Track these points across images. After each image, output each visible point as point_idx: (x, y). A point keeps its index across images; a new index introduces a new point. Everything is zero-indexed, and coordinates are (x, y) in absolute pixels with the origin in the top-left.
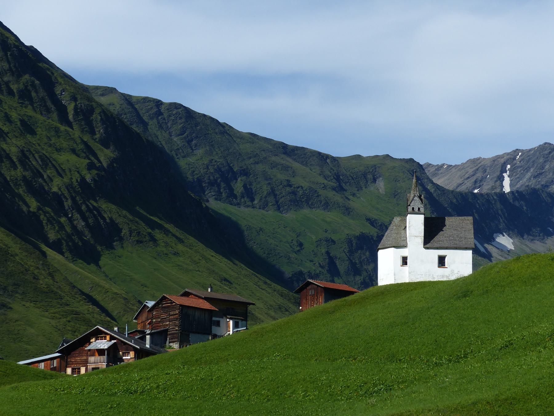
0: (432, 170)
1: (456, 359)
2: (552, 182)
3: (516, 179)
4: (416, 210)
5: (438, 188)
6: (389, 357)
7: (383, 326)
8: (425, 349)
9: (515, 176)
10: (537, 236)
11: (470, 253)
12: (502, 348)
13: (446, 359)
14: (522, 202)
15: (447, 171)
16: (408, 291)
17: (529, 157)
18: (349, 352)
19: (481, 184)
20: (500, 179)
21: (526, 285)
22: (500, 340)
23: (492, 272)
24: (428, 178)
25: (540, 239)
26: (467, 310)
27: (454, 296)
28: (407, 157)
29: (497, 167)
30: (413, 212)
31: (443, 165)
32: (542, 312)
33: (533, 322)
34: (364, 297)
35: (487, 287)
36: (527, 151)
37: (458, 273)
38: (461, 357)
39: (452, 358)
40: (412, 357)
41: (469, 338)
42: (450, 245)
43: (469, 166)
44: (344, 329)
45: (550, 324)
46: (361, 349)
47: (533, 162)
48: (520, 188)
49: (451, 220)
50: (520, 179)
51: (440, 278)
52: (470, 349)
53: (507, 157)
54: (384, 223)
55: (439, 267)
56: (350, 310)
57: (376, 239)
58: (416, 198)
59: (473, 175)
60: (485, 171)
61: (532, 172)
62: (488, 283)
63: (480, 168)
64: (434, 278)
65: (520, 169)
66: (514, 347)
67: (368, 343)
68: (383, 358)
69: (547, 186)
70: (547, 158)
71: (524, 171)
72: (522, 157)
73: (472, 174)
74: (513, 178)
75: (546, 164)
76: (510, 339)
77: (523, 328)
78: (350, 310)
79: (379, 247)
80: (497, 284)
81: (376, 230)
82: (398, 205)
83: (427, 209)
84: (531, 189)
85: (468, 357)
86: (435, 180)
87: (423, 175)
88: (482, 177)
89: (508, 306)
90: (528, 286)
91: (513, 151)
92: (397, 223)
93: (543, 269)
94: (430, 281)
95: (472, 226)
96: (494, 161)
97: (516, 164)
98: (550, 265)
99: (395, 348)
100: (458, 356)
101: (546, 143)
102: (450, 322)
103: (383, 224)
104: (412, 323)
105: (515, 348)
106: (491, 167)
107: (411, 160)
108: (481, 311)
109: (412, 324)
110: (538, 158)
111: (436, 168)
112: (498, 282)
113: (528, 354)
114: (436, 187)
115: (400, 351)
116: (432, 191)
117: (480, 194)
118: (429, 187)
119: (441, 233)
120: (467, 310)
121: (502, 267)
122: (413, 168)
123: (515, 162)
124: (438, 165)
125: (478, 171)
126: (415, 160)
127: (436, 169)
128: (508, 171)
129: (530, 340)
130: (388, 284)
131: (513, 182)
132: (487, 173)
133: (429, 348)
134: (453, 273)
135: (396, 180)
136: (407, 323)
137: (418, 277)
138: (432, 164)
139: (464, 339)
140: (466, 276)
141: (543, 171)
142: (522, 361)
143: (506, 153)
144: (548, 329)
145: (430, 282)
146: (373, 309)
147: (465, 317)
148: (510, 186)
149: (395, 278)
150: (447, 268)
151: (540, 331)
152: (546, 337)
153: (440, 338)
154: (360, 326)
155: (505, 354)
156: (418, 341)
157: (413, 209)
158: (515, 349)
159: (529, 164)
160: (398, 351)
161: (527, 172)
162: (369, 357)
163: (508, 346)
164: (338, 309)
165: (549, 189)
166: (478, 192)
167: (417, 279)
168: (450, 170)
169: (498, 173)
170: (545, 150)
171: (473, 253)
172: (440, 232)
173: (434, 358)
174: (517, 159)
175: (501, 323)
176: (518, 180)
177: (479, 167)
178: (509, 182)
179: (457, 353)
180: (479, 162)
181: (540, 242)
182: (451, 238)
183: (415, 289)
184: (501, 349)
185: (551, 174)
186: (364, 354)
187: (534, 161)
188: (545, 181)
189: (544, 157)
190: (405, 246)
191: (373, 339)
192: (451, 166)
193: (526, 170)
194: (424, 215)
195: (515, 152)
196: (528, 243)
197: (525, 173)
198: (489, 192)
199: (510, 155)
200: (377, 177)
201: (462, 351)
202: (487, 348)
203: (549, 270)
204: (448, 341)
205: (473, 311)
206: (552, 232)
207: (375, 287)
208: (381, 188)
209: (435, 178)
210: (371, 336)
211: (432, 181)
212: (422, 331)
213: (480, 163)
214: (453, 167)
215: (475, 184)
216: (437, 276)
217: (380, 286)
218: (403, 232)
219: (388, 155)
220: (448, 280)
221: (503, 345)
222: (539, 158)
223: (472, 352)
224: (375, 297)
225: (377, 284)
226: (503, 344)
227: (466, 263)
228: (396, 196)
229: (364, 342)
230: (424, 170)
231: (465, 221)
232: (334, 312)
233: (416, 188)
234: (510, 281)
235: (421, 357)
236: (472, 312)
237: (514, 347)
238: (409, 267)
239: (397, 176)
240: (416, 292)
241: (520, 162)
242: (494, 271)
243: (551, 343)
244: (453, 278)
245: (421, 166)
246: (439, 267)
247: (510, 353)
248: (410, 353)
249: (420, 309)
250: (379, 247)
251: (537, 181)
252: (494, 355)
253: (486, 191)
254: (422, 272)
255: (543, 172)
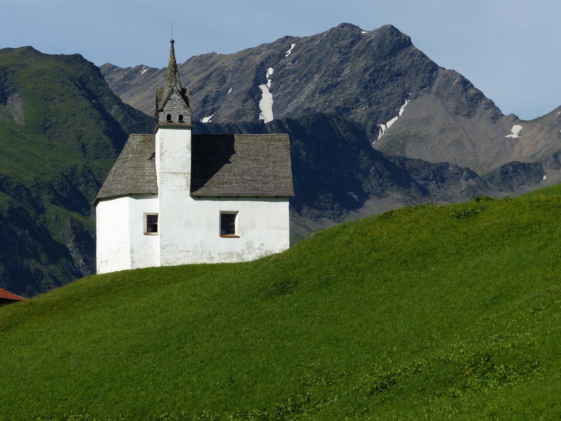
0: (118, 78)
1: (276, 415)
2: (357, 103)
3: (285, 96)
4: (175, 119)
5: (131, 114)
6: (135, 414)
7: (117, 354)
8: (210, 397)
9: (284, 90)
10: (327, 209)
11: (285, 205)
12: (374, 391)
13: (255, 415)
14: (298, 142)
15: (148, 80)
16: (160, 284)
17: (310, 53)
18: (49, 407)
19: (216, 106)
20: (253, 96)
21: (408, 268)
22: (368, 376)
23: (335, 243)
24: (111, 94)
25: (334, 214)
26: (291, 319)
27: (260, 291)
28: (69, 51)
29: (249, 71)
30: (169, 124)
31: (140, 67)
32: (447, 319)
33: (431, 339)
34: (70, 298)
35: (327, 273)
36: (307, 39)
37: (262, 247)
38: (287, 411)
39: (268, 415)
40: (183, 413)
41: (301, 373)
42: (245, 190)
43: (190, 71)
44: (36, 361)
45: (469, 343)
46: (75, 399)
47: (319, 62)
48: (293, 114)
49: (245, 141)
50: (293, 95)
51: (224, 259)
52: (304, 394)
53: (268, 52)
54: (23, 183)
55: (222, 235)
56: (43, 324)
57: (8, 216)
58: (174, 96)
59: (201, 88)
60: (223, 80)
61: (316, 83)
62: (330, 264)
63: (214, 74)
64: (212, 258)
65: (292, 76)
66: (399, 388)
67: (90, 388)
68: (123, 416)
69: (346, 110)
70: (346, 54)
71: (301, 79)
72: (297, 52)
73: (197, 85)
74: (278, 94)
75: (344, 66)
76: (389, 373)
77: (413, 352)
78: (43, 324)
79: (99, 195)
80: (348, 266)
81: (8, 198)
82: (51, 148)
83: (110, 156)
84: (316, 115)
85: (303, 412)
86: (125, 99)
87: (101, 88)
88: (218, 91)
89: (373, 310)
90: (412, 270)
91: (280, 39)
92: (135, 147)
93: (440, 237)
94: (205, 264)
95: (289, 153)
96: (241, 60)
97: (285, 66)
98: (454, 226)
99: (146, 397)
100: (281, 408)
101: (344, 25)
102: (257, 343)
103: (22, 185)
104: (177, 346)
105: (401, 389)
106: (235, 71)
107: (78, 58)
108: (319, 320)
109: (178, 349)
110: (328, 54)
111: (126, 73)
112: (351, 263)
113: (430, 401)
114: (128, 112)
115: (157, 402)
116: (120, 119)
117: (215, 125)
118: (113, 111)
119: (226, 166)
120: (291, 319)
121: (355, 232)
122: (82, 74)
123: (283, 61)
124: (130, 68)
125: (210, 81)
126: (86, 57)
127: (127, 76)
128: (269, 81)
129: (431, 374)
130: (119, 270)
131: (278, 102)
132: (226, 85)
133: (219, 395)
134: (250, 247)
135: (47, 98)
136: (167, 346)
137: (179, 256)
138: (117, 67)
139: (290, 375)
140: (279, 254)
141: (339, 79)
142: (423, 414)
143: (264, 44)
144: (467, 352)
145: (205, 267)
146: (92, 320)
147: (287, 332)
148: (273, 110)
149: (132, 258)
150: (238, 237)
151: (451, 356)
152: (466, 367)
153: (239, 375)
154: (69, 354)
155: (382, 402)
156: (193, 381)
157: (169, 117)
158: (401, 391)
159: (310, 66)
160: (154, 402)
161: (307, 81)
162: (92, 415)
163: (386, 387)
164: (18, 321)
165: (351, 116)
166: (210, 121)
167: (178, 259)
168: (153, 78)
169: (249, 85)
170: (344, 38)
171: (290, 208)
172: (224, 164)
173: (230, 414)
174: (286, 56)
175: (364, 344)
176: (289, 97)
177: (212, 73)
178: (271, 102)
179: (277, 404)
180: (211, 61)
181: (334, 220)
182: (246, 177)
183: (176, 280)
184: (372, 394)
185: (355, 86)
186: (81, 409)
187: (321, 59)
188: (343, 99)
189: (340, 52)
190: (153, 194)
191: (98, 380)
192: (156, 69)
193: (305, 79)
194: (192, 129)
195: (282, 42)
196: (309, 222)
197: (303, 84)
198: (232, 121)
199: (274, 48)
200: (8, 91)
201: (289, 400)
202: (340, 392)
203: (452, 236)
204: (256, 381)
205: (303, 321)
206: (357, 200)
207: (93, 277)
208: (16, 113)
209: (124, 94)
210: (93, 373)
211: (120, 99)
212: (201, 362)
213: (214, 64)
214: (159, 73)
215: (203, 107)
216: (219, 254)
217: (103, 275)
218: (148, 164)
219: (30, 48)
220: (240, 261)
221: (375, 386)
222: (330, 53)
223: (309, 400)
224: (94, 297)
225: (93, 269)
226: (376, 383)
227: (277, 228)
228: (47, 131)
229: (80, 384)
230: (102, 77)
231: (274, 143)
232: (9, 327)
233: (175, 75)
234: (375, 260)
235: (202, 414)
236: (301, 323)
237: (399, 388)
238: (161, 235)
239: (49, 90)
240: (177, 285)
241: (293, 62)
242: (340, 241)
243: (477, 378)
244: (250, 257)
245: (97, 69)
246: (222, 235)
247: (392, 399)
248: (179, 404)
249: (191, 319)
250: (99, 195)
251: (327, 99)
252: (360, 405)
253: (226, 121)
254: (187, 247)
255: (339, 83)
